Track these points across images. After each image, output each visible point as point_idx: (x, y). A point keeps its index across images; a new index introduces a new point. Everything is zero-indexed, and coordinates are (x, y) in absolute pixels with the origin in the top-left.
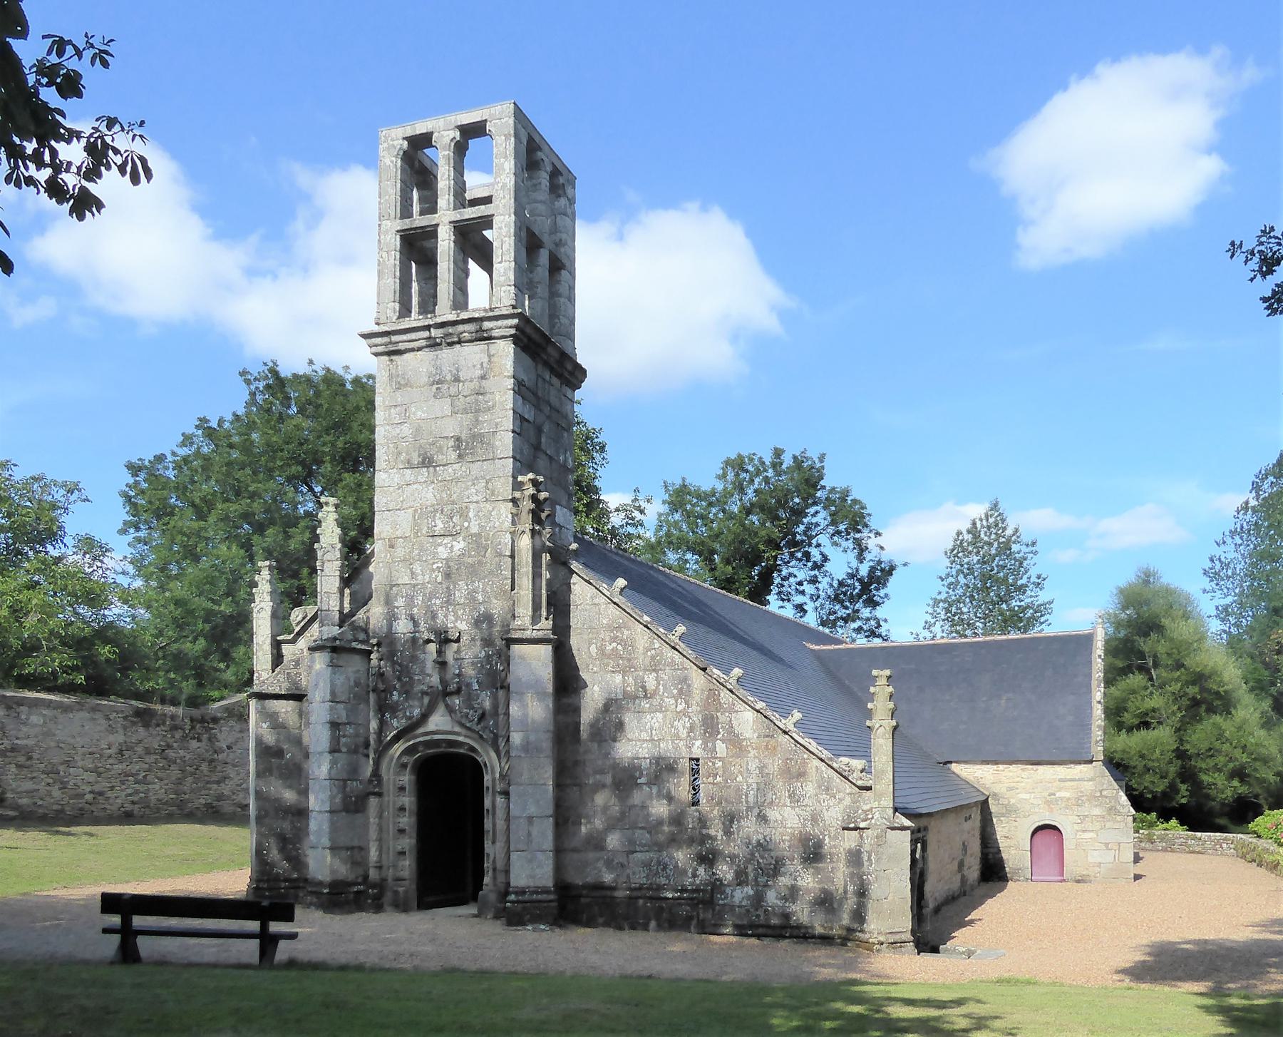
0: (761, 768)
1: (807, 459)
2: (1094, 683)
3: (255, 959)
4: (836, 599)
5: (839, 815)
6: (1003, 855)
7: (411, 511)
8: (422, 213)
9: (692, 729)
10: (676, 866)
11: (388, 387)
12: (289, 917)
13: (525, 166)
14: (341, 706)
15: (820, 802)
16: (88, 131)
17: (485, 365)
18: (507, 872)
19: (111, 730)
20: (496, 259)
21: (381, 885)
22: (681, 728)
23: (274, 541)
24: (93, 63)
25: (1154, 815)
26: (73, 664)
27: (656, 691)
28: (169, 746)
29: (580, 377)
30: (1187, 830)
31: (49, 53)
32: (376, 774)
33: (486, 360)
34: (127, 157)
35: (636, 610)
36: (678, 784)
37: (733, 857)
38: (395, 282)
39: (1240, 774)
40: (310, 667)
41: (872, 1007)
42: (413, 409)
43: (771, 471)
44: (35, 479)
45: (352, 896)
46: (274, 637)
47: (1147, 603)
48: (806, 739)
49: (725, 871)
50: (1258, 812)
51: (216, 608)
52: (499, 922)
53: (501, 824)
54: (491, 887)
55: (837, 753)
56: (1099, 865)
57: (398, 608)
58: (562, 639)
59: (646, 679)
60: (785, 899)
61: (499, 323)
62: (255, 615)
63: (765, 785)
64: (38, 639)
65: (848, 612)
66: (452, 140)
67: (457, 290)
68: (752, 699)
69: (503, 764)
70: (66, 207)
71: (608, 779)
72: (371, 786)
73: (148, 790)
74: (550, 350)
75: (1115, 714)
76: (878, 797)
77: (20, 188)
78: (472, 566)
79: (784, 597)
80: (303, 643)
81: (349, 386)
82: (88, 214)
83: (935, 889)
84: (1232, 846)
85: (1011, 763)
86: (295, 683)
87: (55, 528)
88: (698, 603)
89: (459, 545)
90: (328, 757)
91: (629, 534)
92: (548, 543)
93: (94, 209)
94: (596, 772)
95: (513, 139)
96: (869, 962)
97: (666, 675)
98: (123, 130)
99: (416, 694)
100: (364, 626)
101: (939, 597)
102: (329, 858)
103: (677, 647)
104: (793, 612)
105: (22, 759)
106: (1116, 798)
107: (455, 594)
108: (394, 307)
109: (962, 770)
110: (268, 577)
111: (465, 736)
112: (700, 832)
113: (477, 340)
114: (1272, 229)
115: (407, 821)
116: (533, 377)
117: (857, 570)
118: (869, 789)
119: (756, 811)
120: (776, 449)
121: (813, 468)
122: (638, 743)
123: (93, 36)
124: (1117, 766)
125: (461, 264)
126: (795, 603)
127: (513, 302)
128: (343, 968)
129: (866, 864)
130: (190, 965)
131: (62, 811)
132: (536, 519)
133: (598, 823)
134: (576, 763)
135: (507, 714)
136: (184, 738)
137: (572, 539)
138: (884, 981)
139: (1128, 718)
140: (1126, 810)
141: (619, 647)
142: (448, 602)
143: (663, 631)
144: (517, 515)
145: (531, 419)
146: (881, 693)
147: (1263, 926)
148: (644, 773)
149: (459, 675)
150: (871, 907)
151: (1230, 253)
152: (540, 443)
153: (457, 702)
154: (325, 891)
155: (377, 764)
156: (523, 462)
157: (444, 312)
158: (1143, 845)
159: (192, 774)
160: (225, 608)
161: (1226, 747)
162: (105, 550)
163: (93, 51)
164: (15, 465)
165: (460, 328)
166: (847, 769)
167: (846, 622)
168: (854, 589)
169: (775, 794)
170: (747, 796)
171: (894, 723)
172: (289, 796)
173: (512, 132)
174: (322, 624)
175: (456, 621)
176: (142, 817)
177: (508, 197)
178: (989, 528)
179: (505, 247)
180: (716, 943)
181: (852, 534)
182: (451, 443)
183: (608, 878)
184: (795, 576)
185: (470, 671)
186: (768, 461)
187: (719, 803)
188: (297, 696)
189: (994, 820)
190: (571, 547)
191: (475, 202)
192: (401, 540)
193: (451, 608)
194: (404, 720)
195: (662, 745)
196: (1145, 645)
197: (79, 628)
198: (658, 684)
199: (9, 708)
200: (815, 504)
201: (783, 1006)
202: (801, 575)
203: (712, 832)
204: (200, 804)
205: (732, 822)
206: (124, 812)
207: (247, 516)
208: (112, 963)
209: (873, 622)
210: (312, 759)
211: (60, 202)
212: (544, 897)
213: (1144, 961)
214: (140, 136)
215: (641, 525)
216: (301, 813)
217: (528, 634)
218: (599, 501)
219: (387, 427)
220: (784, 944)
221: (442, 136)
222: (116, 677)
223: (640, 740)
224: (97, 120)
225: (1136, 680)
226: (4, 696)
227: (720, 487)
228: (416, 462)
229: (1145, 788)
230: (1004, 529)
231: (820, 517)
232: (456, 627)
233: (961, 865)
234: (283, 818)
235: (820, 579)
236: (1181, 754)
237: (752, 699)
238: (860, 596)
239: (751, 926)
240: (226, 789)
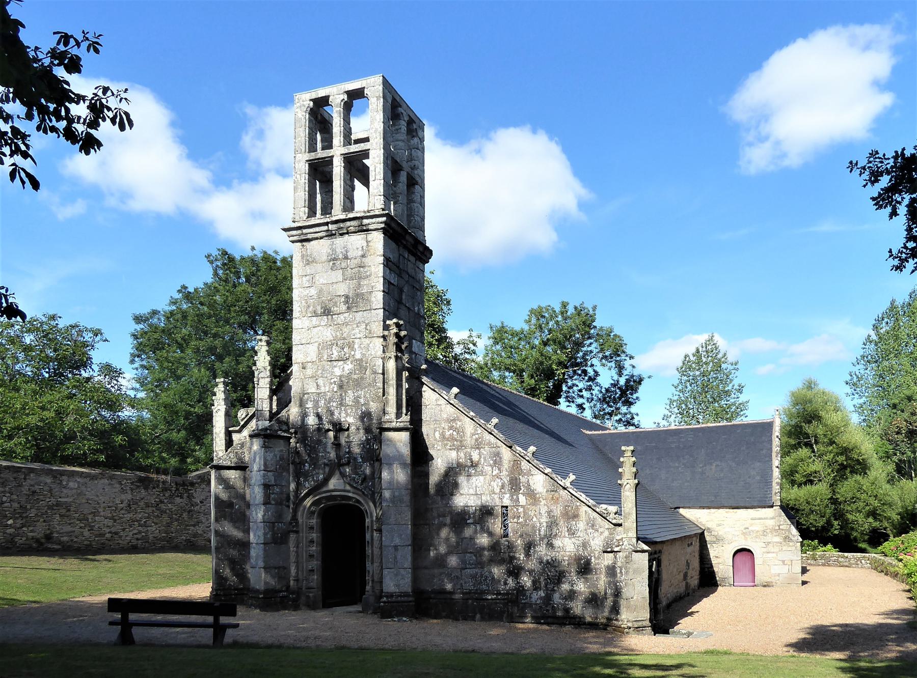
0: (549, 512)
1: (584, 308)
2: (774, 455)
3: (211, 642)
4: (603, 400)
5: (601, 543)
6: (715, 569)
7: (316, 344)
8: (323, 149)
9: (503, 487)
10: (493, 578)
11: (301, 263)
12: (233, 614)
13: (390, 117)
14: (269, 474)
15: (588, 534)
16: (90, 96)
17: (364, 248)
18: (381, 582)
19: (123, 491)
20: (371, 178)
21: (298, 592)
22: (495, 487)
23: (230, 366)
24: (88, 50)
25: (816, 541)
26: (97, 448)
28: (162, 502)
29: (428, 256)
30: (838, 551)
31: (58, 43)
34: (116, 113)
35: (465, 408)
36: (494, 523)
37: (531, 572)
38: (305, 194)
39: (873, 514)
40: (251, 448)
41: (618, 670)
42: (317, 277)
43: (560, 316)
44: (73, 327)
45: (279, 599)
46: (227, 428)
47: (810, 401)
48: (579, 493)
49: (526, 580)
50: (886, 537)
51: (192, 409)
52: (376, 616)
53: (376, 551)
54: (371, 593)
55: (598, 501)
56: (779, 575)
57: (308, 408)
58: (417, 428)
59: (472, 454)
60: (565, 599)
61: (374, 220)
62: (214, 414)
63: (552, 524)
64: (74, 432)
65: (612, 409)
66: (342, 101)
67: (346, 199)
68: (543, 467)
69: (378, 511)
70: (78, 146)
71: (448, 520)
72: (291, 526)
73: (147, 531)
74: (407, 237)
75: (789, 475)
76: (627, 531)
77: (47, 133)
78: (357, 380)
79: (570, 400)
80: (246, 433)
81: (279, 264)
82: (92, 151)
83: (667, 591)
84: (868, 562)
85: (718, 508)
87: (85, 359)
88: (509, 404)
89: (349, 366)
90: (263, 508)
91: (466, 359)
92: (406, 365)
93: (96, 147)
94: (439, 516)
95: (382, 99)
96: (620, 641)
97: (486, 451)
98: (113, 94)
99: (321, 465)
100: (286, 420)
102: (263, 575)
103: (493, 432)
104: (576, 409)
105: (63, 511)
106: (789, 531)
107: (345, 399)
108: (304, 211)
109: (687, 513)
110: (223, 389)
111: (353, 493)
112: (509, 556)
113: (359, 231)
114: (877, 153)
116: (397, 255)
117: (618, 381)
118: (620, 525)
119: (546, 541)
120: (563, 302)
121: (588, 314)
122: (468, 496)
123: (88, 33)
124: (790, 511)
125: (348, 182)
126: (577, 403)
127: (383, 206)
128: (269, 647)
129: (619, 575)
130: (168, 646)
131: (90, 545)
132: (398, 348)
133: (443, 549)
135: (380, 478)
136: (171, 497)
137: (424, 362)
138: (630, 653)
139: (798, 477)
140: (796, 538)
141: (455, 433)
142: (341, 404)
143: (483, 422)
144: (386, 346)
145: (395, 283)
146: (627, 462)
147: (887, 614)
148: (472, 516)
150: (623, 603)
151: (850, 169)
152: (401, 299)
153: (348, 470)
154: (261, 596)
155: (295, 511)
156: (390, 311)
157: (337, 213)
158: (809, 561)
160: (198, 409)
161: (864, 496)
162: (119, 373)
163: (87, 43)
164: (60, 317)
165: (348, 223)
166: (606, 512)
167: (611, 416)
168: (616, 394)
169: (558, 529)
170: (540, 531)
171: (636, 481)
172: (237, 534)
173: (381, 95)
174: (258, 420)
175: (347, 416)
176: (144, 548)
177: (379, 138)
180: (520, 629)
181: (614, 358)
182: (343, 299)
183: (449, 587)
184: (577, 386)
185: (356, 450)
186: (558, 309)
188: (241, 467)
189: (709, 546)
190: (422, 367)
191: (357, 141)
192: (311, 364)
193: (343, 408)
194: (312, 483)
195: (483, 498)
196: (809, 429)
197: (101, 424)
198: (480, 457)
199: (55, 477)
200: (589, 338)
201: (558, 670)
202: (581, 385)
203: (517, 555)
204: (182, 539)
205: (530, 548)
206: (132, 546)
207: (212, 350)
208: (115, 644)
209: (629, 416)
211: (73, 143)
213: (805, 639)
214: (126, 99)
215: (474, 353)
216: (244, 545)
217: (394, 425)
218: (446, 337)
219: (300, 290)
220: (568, 628)
221: (336, 98)
222: (126, 456)
223: (468, 495)
224: (96, 88)
225: (804, 452)
226: (52, 470)
227: (526, 327)
228: (319, 313)
229: (811, 524)
231: (593, 347)
232: (346, 421)
233: (685, 575)
235: (593, 387)
236: (834, 501)
237: (543, 467)
238: (620, 398)
240: (199, 530)
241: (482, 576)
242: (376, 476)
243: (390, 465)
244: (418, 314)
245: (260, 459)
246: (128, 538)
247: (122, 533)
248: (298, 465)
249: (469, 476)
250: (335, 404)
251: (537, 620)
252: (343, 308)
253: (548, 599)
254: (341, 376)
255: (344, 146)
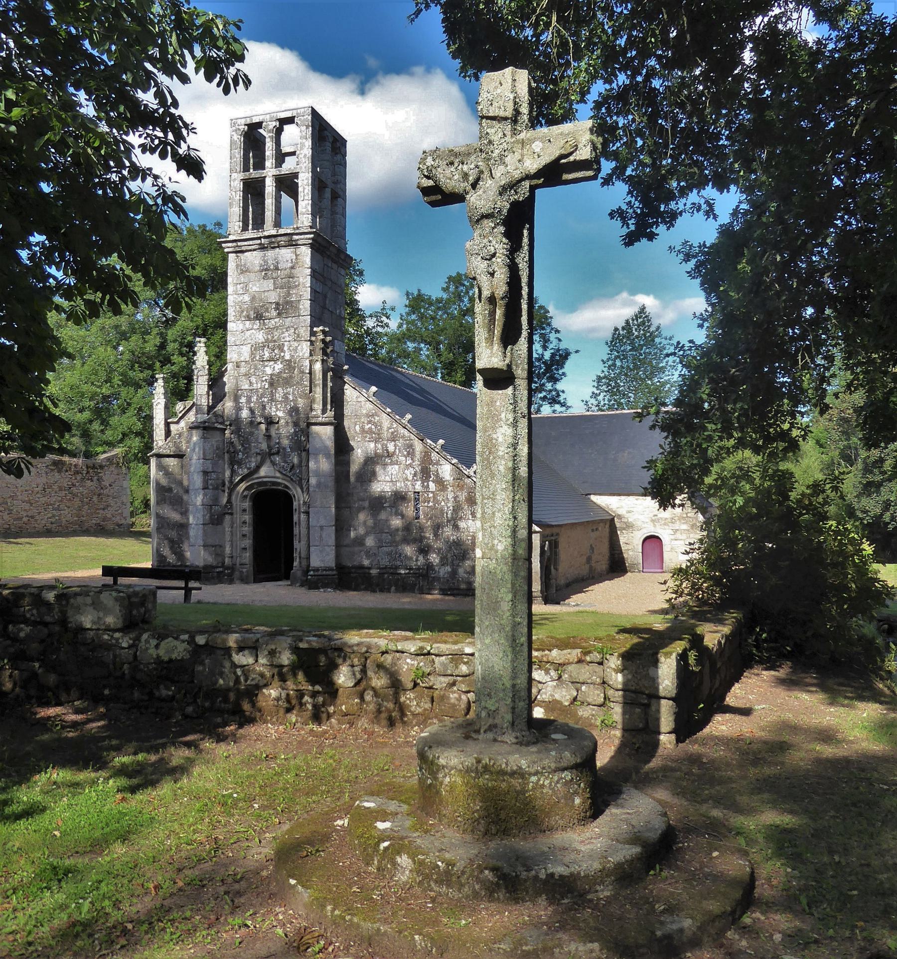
0: (455, 498)
7: (249, 346)
9: (415, 475)
18: (308, 558)
21: (232, 568)
27: (394, 453)
28: (74, 485)
32: (229, 501)
33: (294, 257)
46: (166, 420)
49: (434, 558)
53: (304, 531)
61: (302, 237)
63: (457, 508)
74: (331, 248)
80: (182, 424)
85: (629, 495)
86: (178, 448)
88: (422, 391)
89: (279, 366)
90: (202, 492)
101: (602, 375)
115: (247, 529)
117: (543, 355)
119: (452, 522)
132: (325, 353)
134: (348, 494)
135: (308, 466)
136: (83, 479)
149: (278, 443)
152: (325, 304)
156: (316, 320)
157: (269, 229)
159: (88, 504)
165: (279, 239)
168: (541, 368)
172: (175, 516)
178: (639, 326)
179: (306, 191)
182: (274, 306)
183: (366, 563)
185: (286, 442)
187: (431, 518)
188: (180, 456)
203: (427, 535)
205: (438, 529)
209: (554, 393)
210: (192, 493)
212: (330, 573)
216: (183, 527)
218: (358, 310)
230: (649, 326)
233: (589, 559)
234: (172, 530)
238: (544, 374)
239: (450, 589)
241: (396, 553)
242: (304, 464)
243: (316, 455)
244: (340, 316)
245: (199, 450)
246: (43, 522)
247: (37, 517)
248: (233, 455)
249: (385, 465)
250: (266, 400)
251: (444, 592)
252: (274, 313)
253: (454, 573)
254: (271, 375)
255: (276, 167)
